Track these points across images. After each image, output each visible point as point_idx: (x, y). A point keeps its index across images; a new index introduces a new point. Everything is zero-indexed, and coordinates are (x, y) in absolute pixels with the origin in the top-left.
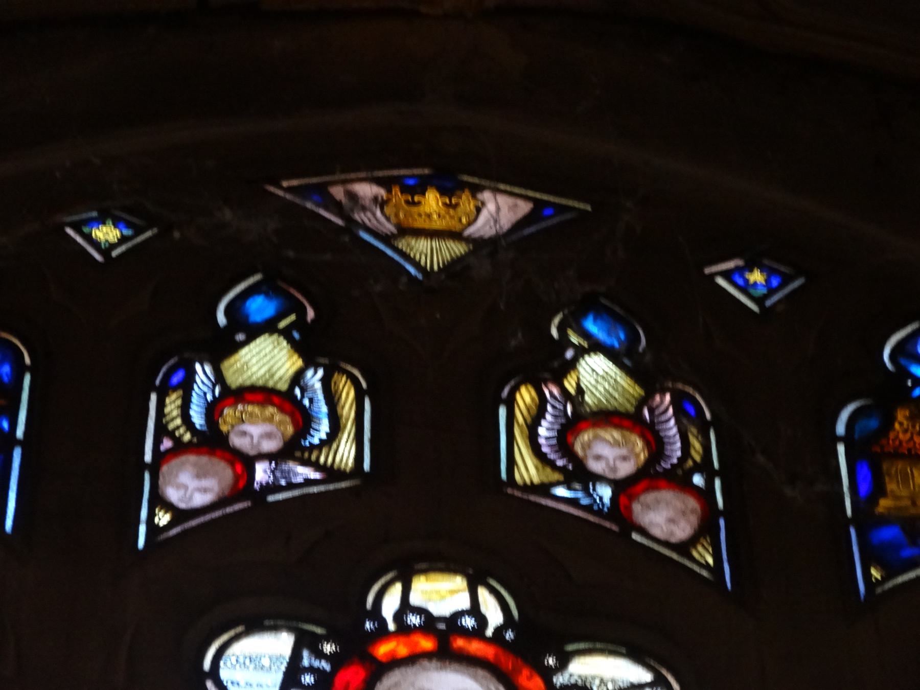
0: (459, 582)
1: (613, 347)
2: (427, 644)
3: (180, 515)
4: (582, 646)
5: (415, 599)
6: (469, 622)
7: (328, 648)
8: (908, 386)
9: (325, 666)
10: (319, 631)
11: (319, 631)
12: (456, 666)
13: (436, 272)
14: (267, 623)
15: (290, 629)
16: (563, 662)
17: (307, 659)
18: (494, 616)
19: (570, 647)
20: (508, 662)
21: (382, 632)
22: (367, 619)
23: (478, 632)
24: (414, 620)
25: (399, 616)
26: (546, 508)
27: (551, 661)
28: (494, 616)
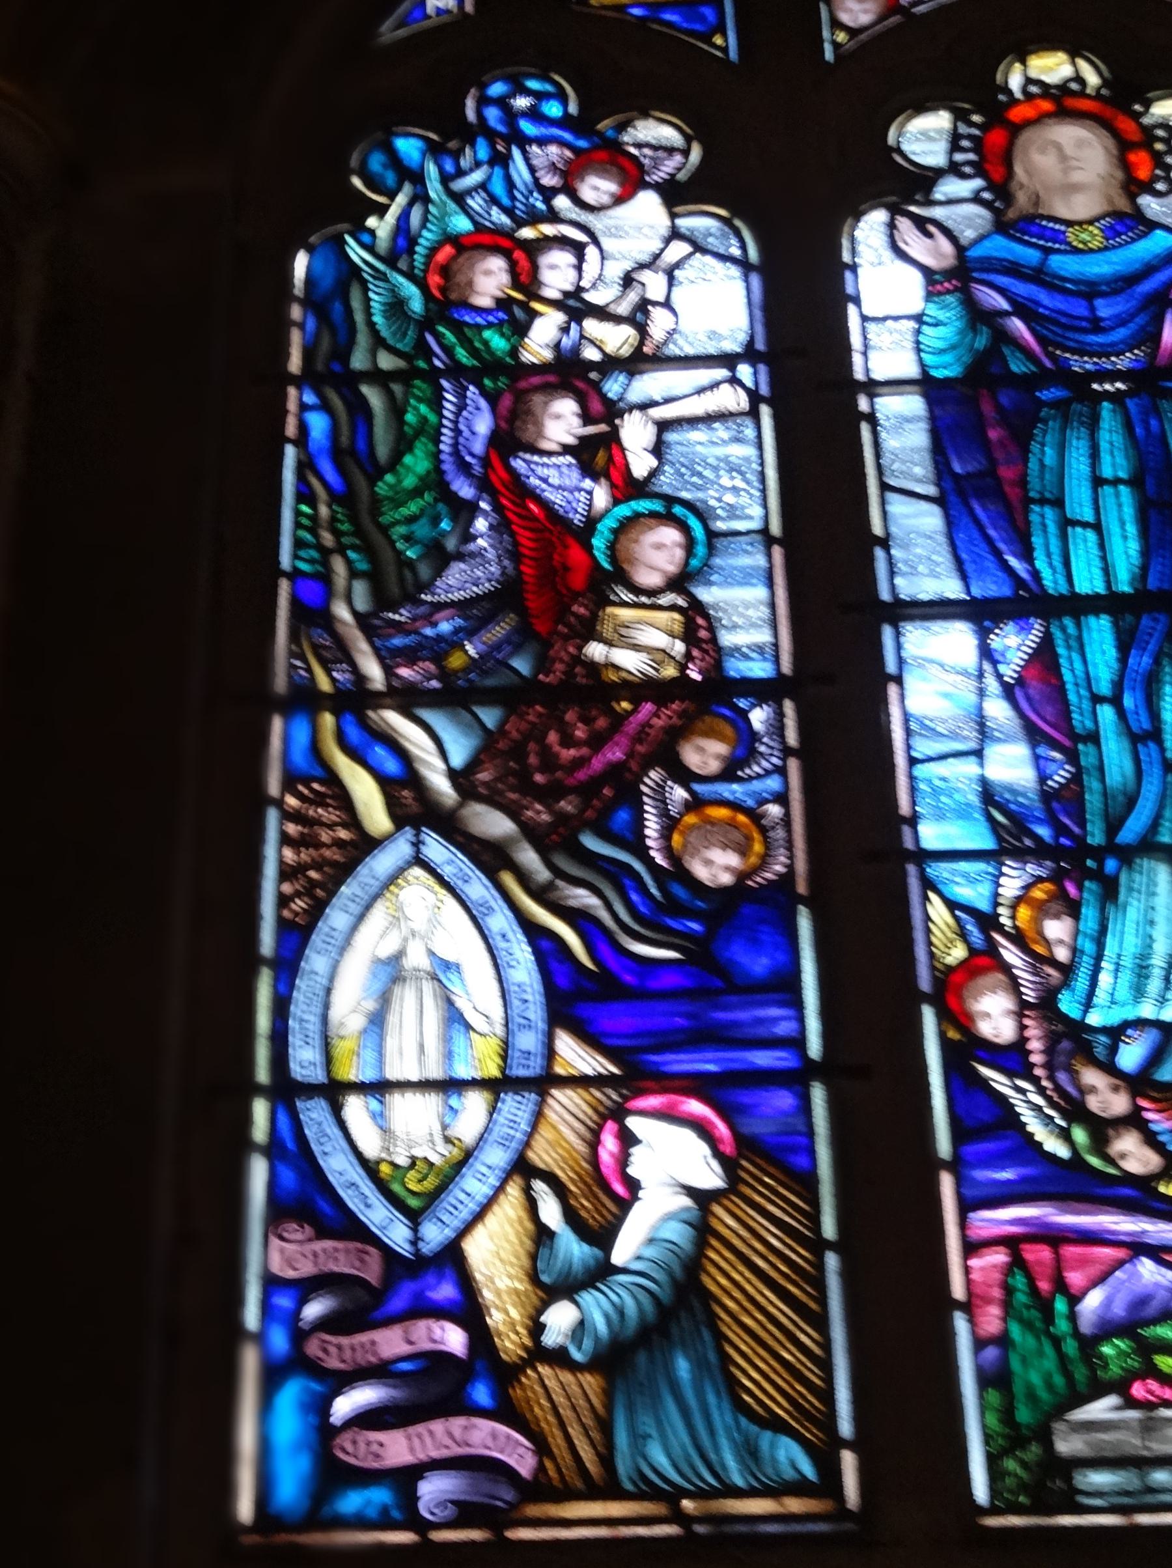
0: (1061, 56)
1: (319, 572)
2: (1046, 106)
3: (853, 32)
4: (1158, 93)
5: (1033, 74)
6: (1074, 86)
7: (976, 118)
8: (828, 63)
9: (976, 132)
10: (967, 106)
11: (967, 106)
12: (1068, 120)
13: (737, 1184)
14: (928, 104)
15: (945, 108)
16: (1147, 104)
17: (963, 129)
18: (1092, 79)
19: (1150, 95)
20: (1108, 112)
21: (1014, 102)
22: (1133, 386)
23: (1082, 94)
24: (1034, 89)
25: (1024, 91)
26: (701, 48)
27: (1137, 107)
28: (1092, 79)
